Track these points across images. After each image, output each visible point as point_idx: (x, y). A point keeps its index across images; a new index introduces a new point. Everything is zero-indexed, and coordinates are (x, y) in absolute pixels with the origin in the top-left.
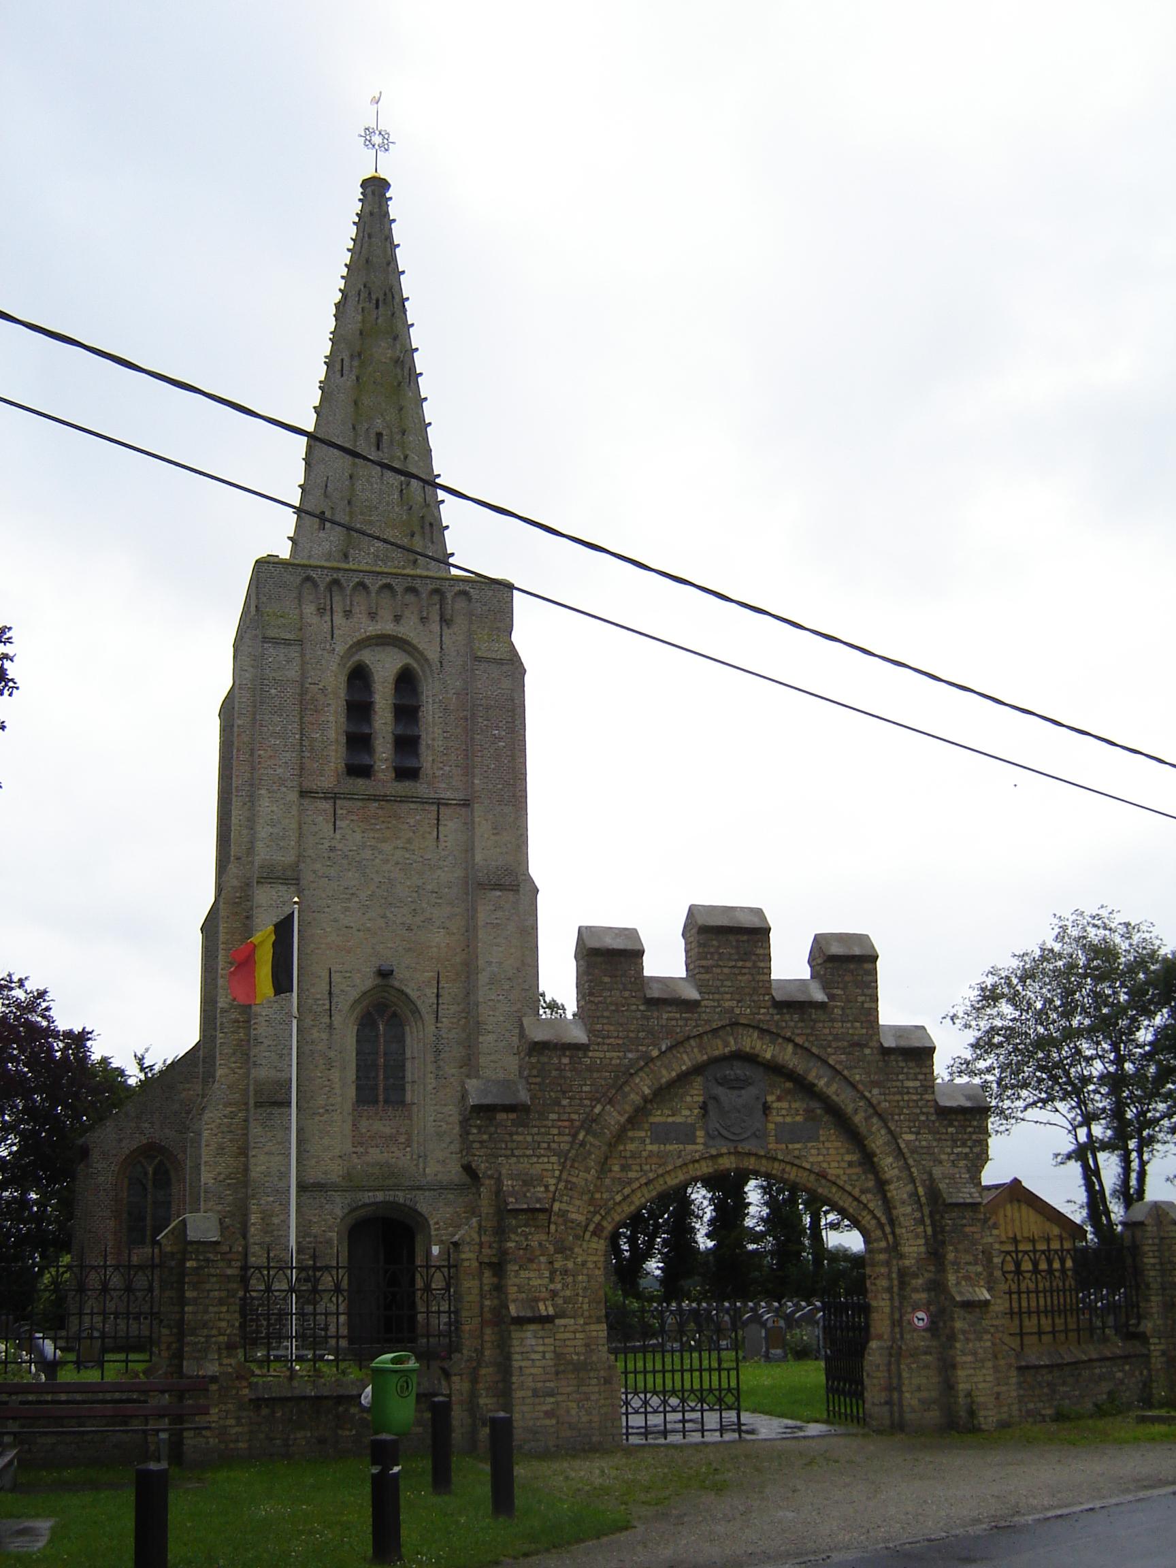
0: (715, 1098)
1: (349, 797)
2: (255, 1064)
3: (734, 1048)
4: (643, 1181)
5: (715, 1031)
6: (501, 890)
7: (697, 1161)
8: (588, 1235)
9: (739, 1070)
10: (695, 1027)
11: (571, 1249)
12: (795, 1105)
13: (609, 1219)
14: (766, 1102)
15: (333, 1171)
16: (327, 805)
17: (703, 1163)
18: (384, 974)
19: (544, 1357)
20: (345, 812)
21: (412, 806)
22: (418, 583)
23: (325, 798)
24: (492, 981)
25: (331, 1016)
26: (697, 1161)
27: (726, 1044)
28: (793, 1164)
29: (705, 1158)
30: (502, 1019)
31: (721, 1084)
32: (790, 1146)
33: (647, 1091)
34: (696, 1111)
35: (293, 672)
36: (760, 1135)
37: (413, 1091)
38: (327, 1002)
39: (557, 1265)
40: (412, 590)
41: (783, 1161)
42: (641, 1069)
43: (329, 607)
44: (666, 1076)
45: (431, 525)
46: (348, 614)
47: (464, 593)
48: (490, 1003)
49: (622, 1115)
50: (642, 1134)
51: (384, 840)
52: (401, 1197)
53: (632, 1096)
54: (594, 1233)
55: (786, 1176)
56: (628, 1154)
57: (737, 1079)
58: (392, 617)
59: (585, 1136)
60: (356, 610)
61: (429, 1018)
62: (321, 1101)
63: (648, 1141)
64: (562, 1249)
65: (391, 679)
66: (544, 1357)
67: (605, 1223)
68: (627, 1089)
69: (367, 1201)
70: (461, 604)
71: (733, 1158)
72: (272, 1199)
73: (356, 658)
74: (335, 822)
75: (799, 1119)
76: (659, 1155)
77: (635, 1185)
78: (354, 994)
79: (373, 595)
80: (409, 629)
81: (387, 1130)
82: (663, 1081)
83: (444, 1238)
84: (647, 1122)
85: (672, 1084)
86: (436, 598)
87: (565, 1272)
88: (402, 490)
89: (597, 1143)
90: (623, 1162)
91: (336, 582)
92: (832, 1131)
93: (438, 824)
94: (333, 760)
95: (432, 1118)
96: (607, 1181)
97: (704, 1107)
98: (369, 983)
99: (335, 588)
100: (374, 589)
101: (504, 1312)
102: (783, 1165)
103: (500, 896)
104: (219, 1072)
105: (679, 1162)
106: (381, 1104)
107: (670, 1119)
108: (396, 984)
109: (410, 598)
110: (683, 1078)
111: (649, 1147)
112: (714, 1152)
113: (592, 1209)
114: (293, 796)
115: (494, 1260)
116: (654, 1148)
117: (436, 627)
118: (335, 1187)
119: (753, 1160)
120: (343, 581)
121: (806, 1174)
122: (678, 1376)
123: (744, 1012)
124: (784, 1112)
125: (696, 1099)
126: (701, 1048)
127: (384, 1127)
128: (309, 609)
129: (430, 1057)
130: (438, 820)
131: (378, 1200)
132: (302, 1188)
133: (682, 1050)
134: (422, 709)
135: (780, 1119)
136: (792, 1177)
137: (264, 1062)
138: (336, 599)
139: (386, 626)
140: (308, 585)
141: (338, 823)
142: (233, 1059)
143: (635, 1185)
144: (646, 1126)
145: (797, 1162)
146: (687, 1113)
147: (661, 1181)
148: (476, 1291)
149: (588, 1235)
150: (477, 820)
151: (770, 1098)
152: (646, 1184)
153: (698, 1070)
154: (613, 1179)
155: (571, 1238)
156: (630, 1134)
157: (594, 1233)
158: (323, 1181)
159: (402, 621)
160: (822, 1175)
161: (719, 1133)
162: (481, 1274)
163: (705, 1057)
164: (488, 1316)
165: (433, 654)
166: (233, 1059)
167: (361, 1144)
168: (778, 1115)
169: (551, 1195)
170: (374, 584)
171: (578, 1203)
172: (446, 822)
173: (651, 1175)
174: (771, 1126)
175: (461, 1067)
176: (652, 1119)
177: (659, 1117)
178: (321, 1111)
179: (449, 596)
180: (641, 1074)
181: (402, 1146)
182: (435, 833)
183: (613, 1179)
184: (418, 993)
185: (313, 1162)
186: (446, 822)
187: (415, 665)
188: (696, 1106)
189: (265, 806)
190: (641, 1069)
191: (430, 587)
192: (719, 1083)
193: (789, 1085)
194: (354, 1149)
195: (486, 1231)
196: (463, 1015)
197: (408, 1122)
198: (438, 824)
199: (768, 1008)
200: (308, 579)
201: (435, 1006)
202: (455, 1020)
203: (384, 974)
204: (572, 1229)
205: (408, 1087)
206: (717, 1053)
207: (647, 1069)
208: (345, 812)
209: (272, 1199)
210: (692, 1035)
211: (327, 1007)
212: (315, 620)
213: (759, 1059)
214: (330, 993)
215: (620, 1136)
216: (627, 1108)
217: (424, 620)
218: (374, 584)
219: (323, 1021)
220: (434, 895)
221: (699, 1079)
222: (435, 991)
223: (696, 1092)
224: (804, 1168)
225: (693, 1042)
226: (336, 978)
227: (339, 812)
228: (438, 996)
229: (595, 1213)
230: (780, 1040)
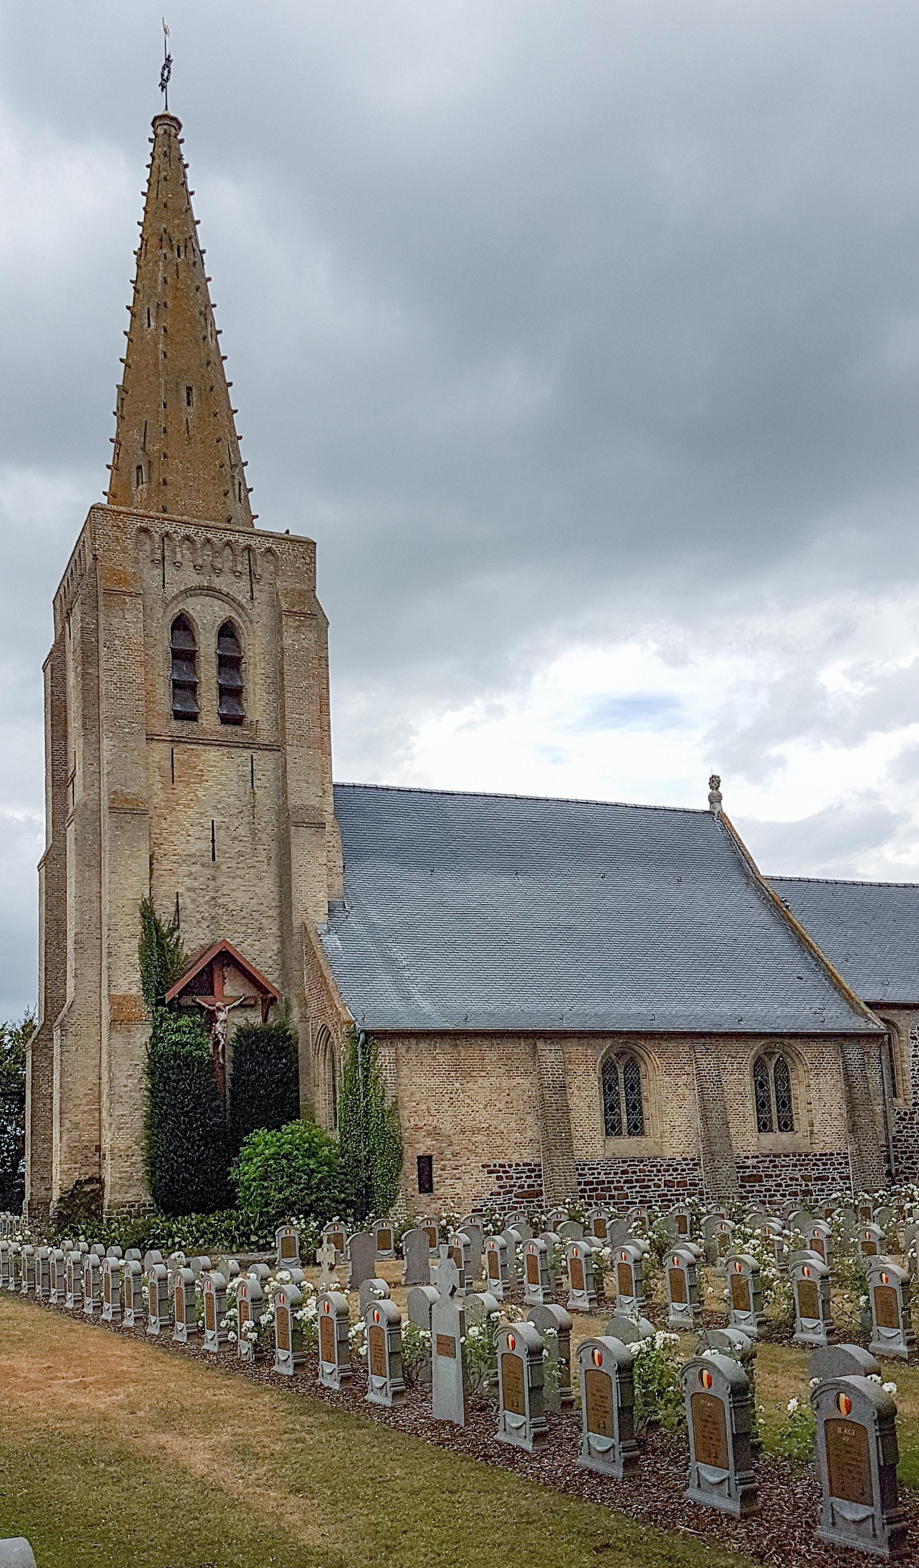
45: (240, 484)
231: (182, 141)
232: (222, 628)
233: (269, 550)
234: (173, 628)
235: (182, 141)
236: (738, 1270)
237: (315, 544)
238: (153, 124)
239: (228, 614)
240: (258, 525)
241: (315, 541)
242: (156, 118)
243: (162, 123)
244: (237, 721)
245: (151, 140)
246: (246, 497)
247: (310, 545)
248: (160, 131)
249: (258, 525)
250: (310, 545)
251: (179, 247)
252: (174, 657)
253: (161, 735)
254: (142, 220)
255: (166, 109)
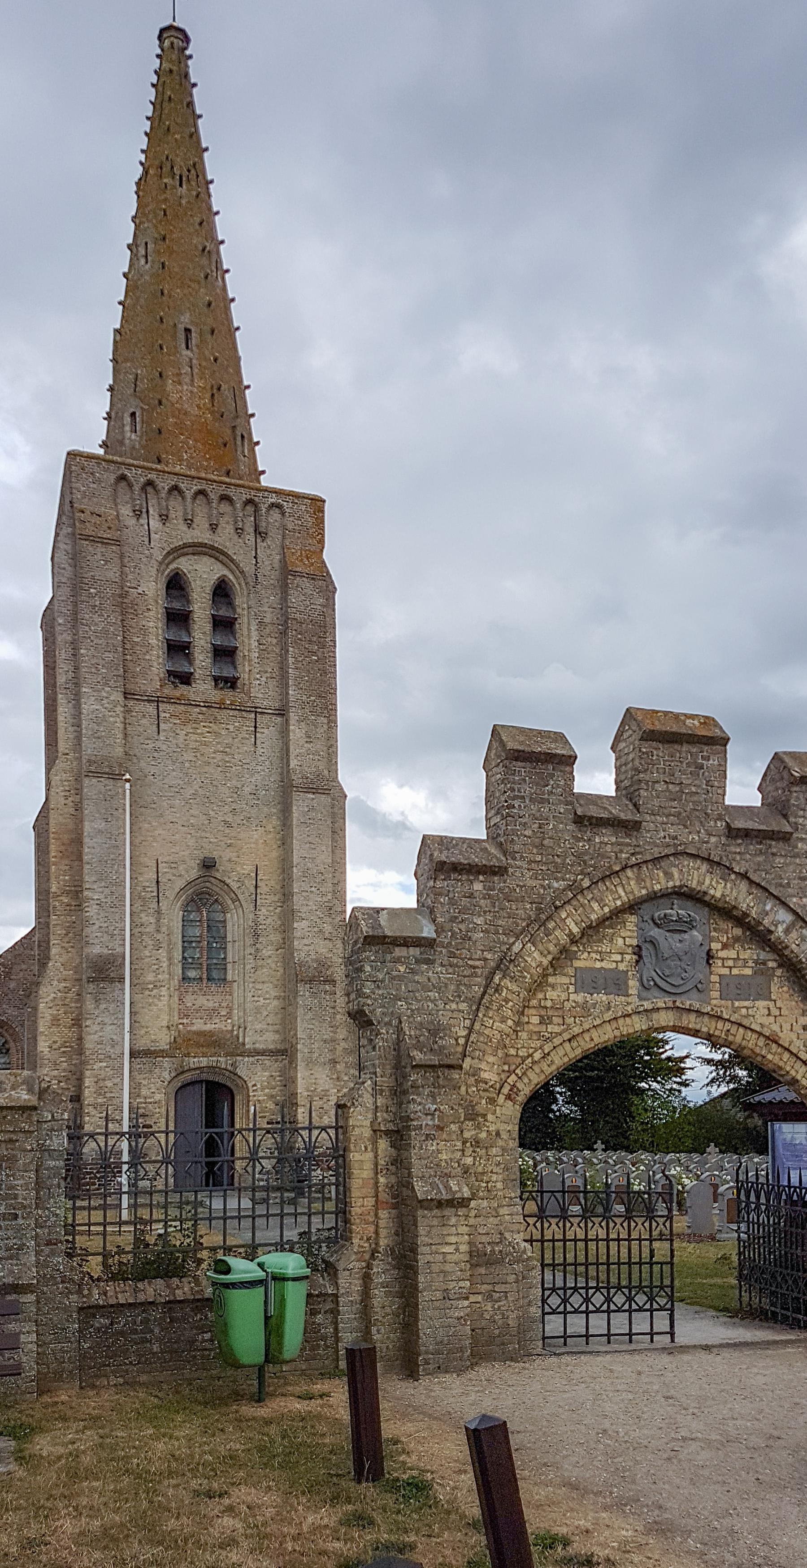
0: (652, 942)
1: (169, 700)
2: (87, 943)
3: (678, 884)
4: (566, 1036)
5: (656, 860)
6: (314, 793)
7: (629, 1015)
8: (502, 1098)
9: (678, 910)
10: (633, 854)
11: (484, 1116)
12: (746, 955)
13: (526, 1080)
14: (710, 950)
15: (163, 1040)
16: (151, 709)
17: (635, 1018)
18: (208, 865)
19: (457, 1250)
20: (168, 715)
21: (231, 713)
22: (231, 492)
23: (149, 701)
24: (305, 873)
25: (158, 902)
26: (629, 1015)
27: (668, 875)
28: (740, 1025)
29: (639, 1012)
30: (314, 908)
31: (658, 926)
32: (737, 1004)
33: (575, 930)
34: (628, 957)
35: (112, 573)
36: (700, 989)
37: (234, 970)
38: (155, 889)
39: (467, 1135)
40: (225, 498)
41: (729, 1020)
42: (569, 901)
43: (144, 510)
44: (597, 912)
45: (243, 437)
46: (164, 518)
47: (279, 506)
48: (303, 894)
49: (545, 956)
50: (565, 980)
51: (205, 744)
52: (223, 1062)
53: (558, 933)
54: (508, 1097)
55: (731, 1038)
56: (549, 1004)
57: (680, 920)
58: (207, 526)
59: (501, 979)
60: (172, 515)
61: (249, 907)
62: (150, 977)
63: (572, 989)
64: (473, 1115)
65: (209, 590)
66: (457, 1250)
67: (520, 1085)
68: (551, 925)
69: (192, 1066)
70: (275, 515)
71: (670, 1014)
72: (105, 1064)
73: (172, 567)
74: (158, 724)
75: (748, 972)
76: (584, 1006)
77: (557, 1041)
78: (181, 883)
79: (189, 500)
80: (225, 538)
81: (211, 1005)
82: (593, 917)
83: (260, 1098)
84: (572, 966)
85: (603, 921)
86: (250, 509)
87: (477, 1143)
88: (213, 395)
89: (515, 988)
90: (543, 1013)
91: (150, 483)
92: (785, 989)
93: (255, 731)
94: (155, 664)
95: (252, 993)
96: (524, 1035)
97: (638, 951)
98: (194, 873)
99: (149, 489)
100: (189, 495)
101: (406, 1192)
102: (728, 1026)
103: (313, 799)
104: (54, 951)
105: (608, 1016)
106: (205, 981)
107: (598, 965)
108: (218, 875)
109: (225, 507)
110: (617, 914)
111: (572, 997)
112: (647, 1005)
113: (506, 1068)
114: (118, 696)
115: (391, 1127)
116: (580, 998)
117: (250, 537)
118: (162, 1053)
119: (692, 1017)
120: (157, 482)
121: (755, 1036)
122: (570, 1258)
123: (691, 838)
124: (730, 963)
125: (628, 941)
126: (639, 880)
127: (205, 1002)
128: (126, 511)
129: (249, 941)
130: (255, 727)
131: (202, 1065)
132: (132, 1055)
133: (616, 881)
134: (239, 621)
135: (726, 971)
136: (738, 1039)
137: (96, 941)
138: (152, 502)
139: (200, 534)
140: (123, 484)
141: (162, 726)
142: (66, 940)
143: (557, 1041)
144: (571, 972)
145: (745, 1022)
146: (618, 958)
147: (587, 1037)
148: (368, 1166)
149: (502, 1098)
150: (292, 727)
151: (715, 946)
152: (570, 1040)
153: (632, 907)
154: (531, 1033)
155: (484, 1101)
156: (551, 980)
157: (508, 1097)
158: (152, 1049)
159: (219, 530)
160: (773, 1039)
161: (656, 984)
162: (375, 1143)
163: (644, 892)
164: (384, 1196)
165: (248, 567)
166: (66, 940)
167: (187, 1016)
168: (723, 966)
169: (460, 1049)
170: (190, 488)
171: (491, 1059)
172: (262, 730)
173: (577, 1030)
174: (714, 978)
175: (277, 950)
176: (577, 964)
177: (585, 960)
178: (151, 986)
179: (263, 508)
180: (568, 908)
181: (223, 1019)
182: (253, 740)
183: (531, 1033)
184: (239, 884)
185: (143, 1032)
186: (262, 730)
187: (231, 577)
188: (630, 950)
189: (89, 706)
190: (569, 901)
191: (244, 497)
192: (655, 923)
193: (738, 931)
194: (181, 1021)
195: (382, 1091)
196: (279, 904)
197: (230, 997)
198: (255, 731)
199: (719, 836)
200: (123, 478)
201: (254, 896)
202: (271, 909)
203: (208, 865)
204: (484, 1090)
205: (229, 966)
206: (657, 887)
207: (574, 902)
208: (168, 715)
209: (105, 1064)
210: (630, 863)
211: (155, 894)
212: (131, 522)
213: (707, 898)
214: (158, 882)
215: (540, 984)
216: (552, 948)
217: (239, 531)
218: (190, 488)
219: (152, 906)
220: (253, 796)
221: (633, 919)
222: (254, 882)
223: (629, 933)
224: (752, 1030)
225: (629, 872)
226: (163, 868)
227: (162, 715)
228: (256, 887)
229: (510, 1072)
230: (733, 876)
231: (190, 57)
232: (216, 589)
233: (201, 492)
234: (168, 588)
235: (190, 57)
236: (261, 1115)
237: (324, 501)
238: (160, 37)
239: (221, 573)
240: (264, 481)
241: (324, 497)
242: (162, 31)
243: (176, 35)
244: (231, 683)
245: (158, 56)
246: (254, 451)
247: (317, 504)
248: (167, 43)
249: (264, 481)
250: (317, 504)
251: (181, 177)
252: (168, 620)
253: (134, 694)
254: (145, 148)
255: (174, 20)
